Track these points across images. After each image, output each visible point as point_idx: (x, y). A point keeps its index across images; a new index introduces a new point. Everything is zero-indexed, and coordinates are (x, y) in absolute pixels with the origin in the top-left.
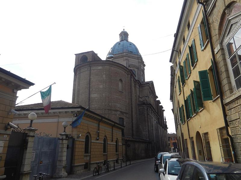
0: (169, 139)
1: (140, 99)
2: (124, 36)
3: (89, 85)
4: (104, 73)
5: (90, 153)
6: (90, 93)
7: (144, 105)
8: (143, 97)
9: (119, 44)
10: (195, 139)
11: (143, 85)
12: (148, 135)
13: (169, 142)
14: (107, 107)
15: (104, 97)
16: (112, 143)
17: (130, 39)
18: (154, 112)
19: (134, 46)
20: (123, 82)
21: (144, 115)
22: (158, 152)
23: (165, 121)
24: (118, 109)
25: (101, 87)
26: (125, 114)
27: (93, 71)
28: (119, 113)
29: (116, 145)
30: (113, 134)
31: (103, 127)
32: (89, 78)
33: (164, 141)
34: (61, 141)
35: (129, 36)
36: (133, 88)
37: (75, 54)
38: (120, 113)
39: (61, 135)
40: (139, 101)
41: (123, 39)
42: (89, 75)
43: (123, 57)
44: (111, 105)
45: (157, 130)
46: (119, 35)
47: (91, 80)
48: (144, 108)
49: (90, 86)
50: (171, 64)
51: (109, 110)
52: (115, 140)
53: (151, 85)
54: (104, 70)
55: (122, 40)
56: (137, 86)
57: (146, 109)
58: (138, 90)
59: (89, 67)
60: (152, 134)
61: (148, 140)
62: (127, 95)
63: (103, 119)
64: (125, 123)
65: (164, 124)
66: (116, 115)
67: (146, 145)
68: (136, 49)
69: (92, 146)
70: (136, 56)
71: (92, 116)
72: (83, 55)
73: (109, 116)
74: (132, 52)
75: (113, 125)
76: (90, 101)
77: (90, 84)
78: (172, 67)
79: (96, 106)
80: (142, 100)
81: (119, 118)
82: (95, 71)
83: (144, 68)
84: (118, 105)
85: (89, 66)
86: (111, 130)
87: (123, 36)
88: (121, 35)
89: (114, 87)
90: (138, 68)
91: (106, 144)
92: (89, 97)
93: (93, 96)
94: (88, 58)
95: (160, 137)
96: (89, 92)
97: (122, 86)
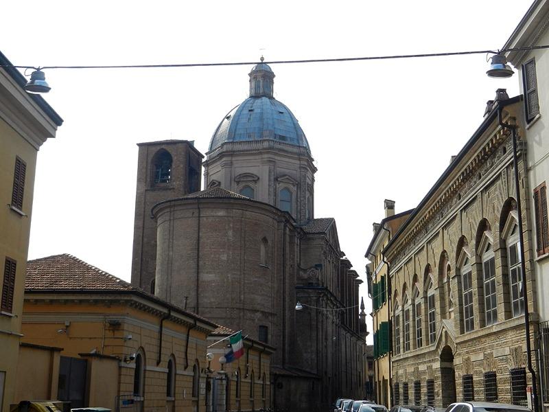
1: (301, 273)
2: (263, 82)
3: (197, 252)
5: (143, 396)
6: (200, 271)
7: (310, 291)
8: (310, 268)
9: (250, 111)
11: (311, 236)
12: (316, 362)
14: (236, 303)
15: (230, 281)
16: (157, 369)
17: (281, 92)
18: (332, 302)
19: (288, 120)
21: (310, 313)
22: (336, 399)
23: (360, 311)
24: (258, 307)
25: (224, 257)
26: (270, 318)
28: (259, 315)
29: (169, 375)
30: (161, 334)
32: (196, 236)
35: (275, 79)
36: (287, 244)
37: (138, 145)
38: (261, 315)
39: (219, 373)
40: (300, 278)
42: (197, 229)
43: (261, 153)
44: (244, 298)
45: (337, 344)
46: (250, 75)
47: (201, 241)
48: (310, 297)
49: (198, 254)
50: (368, 262)
51: (240, 309)
52: (165, 358)
53: (330, 226)
54: (230, 219)
55: (255, 96)
56: (297, 241)
57: (315, 298)
58: (296, 249)
59: (197, 210)
60: (324, 358)
61: (315, 372)
62: (275, 272)
63: (254, 345)
65: (357, 323)
67: (311, 383)
68: (299, 135)
69: (146, 387)
70: (295, 150)
72: (158, 148)
74: (283, 138)
76: (200, 289)
77: (198, 248)
79: (212, 300)
80: (306, 276)
81: (260, 326)
83: (313, 180)
84: (259, 299)
85: (196, 206)
86: (257, 358)
89: (251, 259)
90: (298, 185)
91: (142, 372)
93: (207, 277)
94: (175, 158)
95: (344, 362)
97: (267, 252)
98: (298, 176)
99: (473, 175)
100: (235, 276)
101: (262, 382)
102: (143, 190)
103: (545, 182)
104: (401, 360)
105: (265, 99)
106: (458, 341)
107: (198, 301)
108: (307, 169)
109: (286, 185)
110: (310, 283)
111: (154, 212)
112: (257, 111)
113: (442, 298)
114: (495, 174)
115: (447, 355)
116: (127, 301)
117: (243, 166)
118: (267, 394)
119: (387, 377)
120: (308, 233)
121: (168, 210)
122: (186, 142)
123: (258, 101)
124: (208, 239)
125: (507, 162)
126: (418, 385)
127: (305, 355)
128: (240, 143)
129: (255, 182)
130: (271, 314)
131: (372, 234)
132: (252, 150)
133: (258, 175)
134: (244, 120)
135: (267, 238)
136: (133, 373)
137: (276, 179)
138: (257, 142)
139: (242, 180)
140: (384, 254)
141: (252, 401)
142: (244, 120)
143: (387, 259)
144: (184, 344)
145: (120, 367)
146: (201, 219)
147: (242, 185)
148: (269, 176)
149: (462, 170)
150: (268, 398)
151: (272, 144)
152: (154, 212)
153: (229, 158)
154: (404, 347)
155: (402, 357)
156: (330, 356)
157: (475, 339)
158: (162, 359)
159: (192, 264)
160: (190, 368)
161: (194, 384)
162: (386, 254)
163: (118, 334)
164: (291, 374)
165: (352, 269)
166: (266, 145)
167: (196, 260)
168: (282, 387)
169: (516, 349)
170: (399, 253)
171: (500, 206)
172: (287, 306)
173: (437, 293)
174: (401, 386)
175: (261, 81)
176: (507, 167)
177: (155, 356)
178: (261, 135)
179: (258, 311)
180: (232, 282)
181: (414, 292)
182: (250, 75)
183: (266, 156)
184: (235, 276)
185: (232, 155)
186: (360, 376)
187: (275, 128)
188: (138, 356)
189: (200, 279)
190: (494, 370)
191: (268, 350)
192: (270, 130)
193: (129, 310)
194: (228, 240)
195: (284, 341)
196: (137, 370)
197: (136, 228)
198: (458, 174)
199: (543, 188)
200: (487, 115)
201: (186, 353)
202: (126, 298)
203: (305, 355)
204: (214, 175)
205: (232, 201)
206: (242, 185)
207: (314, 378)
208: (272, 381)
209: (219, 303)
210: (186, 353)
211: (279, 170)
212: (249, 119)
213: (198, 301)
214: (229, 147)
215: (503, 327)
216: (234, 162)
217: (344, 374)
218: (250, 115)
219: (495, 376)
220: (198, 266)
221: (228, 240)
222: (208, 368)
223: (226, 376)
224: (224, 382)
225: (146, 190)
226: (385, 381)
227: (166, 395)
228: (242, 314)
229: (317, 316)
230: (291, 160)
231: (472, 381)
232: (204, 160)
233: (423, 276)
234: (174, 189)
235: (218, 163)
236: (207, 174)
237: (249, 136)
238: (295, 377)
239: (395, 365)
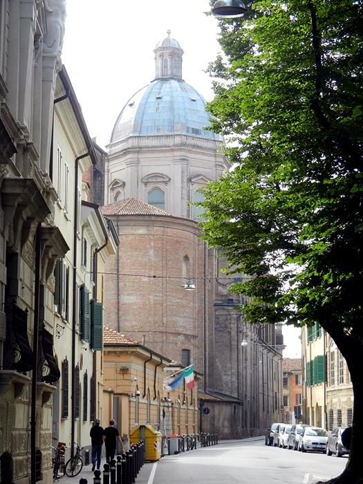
0: (285, 381)
1: (220, 288)
4: (152, 244)
6: (120, 292)
9: (158, 98)
10: (315, 410)
12: (236, 384)
13: (285, 392)
14: (159, 326)
20: (191, 259)
21: (230, 333)
24: (181, 330)
26: (192, 340)
27: (124, 237)
28: (181, 338)
43: (172, 150)
47: (121, 261)
48: (230, 315)
51: (162, 332)
57: (235, 316)
61: (236, 396)
66: (176, 344)
73: (163, 346)
75: (154, 360)
76: (121, 313)
79: (134, 323)
80: (225, 291)
81: (183, 350)
82: (130, 238)
87: (166, 60)
92: (118, 302)
93: (126, 299)
97: (188, 270)
98: (214, 175)
100: (157, 298)
101: (146, 402)
104: (335, 390)
105: (174, 83)
107: (119, 325)
108: (222, 166)
110: (229, 300)
112: (166, 98)
116: (132, 352)
117: (153, 165)
119: (322, 404)
123: (166, 85)
129: (166, 183)
130: (194, 337)
132: (161, 147)
133: (169, 175)
134: (151, 110)
137: (190, 180)
138: (167, 136)
139: (150, 180)
141: (187, 427)
142: (151, 110)
145: (130, 401)
147: (150, 187)
148: (182, 177)
150: (196, 423)
151: (184, 139)
153: (136, 155)
155: (336, 389)
156: (249, 376)
163: (126, 377)
164: (215, 399)
166: (178, 140)
175: (169, 60)
178: (172, 129)
179: (181, 334)
180: (155, 304)
182: (155, 51)
183: (177, 154)
184: (157, 298)
185: (138, 152)
186: (276, 398)
187: (187, 120)
192: (182, 123)
193: (133, 358)
202: (133, 350)
203: (224, 377)
204: (117, 173)
205: (153, 218)
206: (150, 187)
207: (235, 402)
209: (141, 327)
211: (194, 170)
212: (157, 109)
213: (119, 325)
214: (135, 143)
216: (142, 160)
217: (261, 396)
218: (159, 104)
221: (149, 260)
226: (318, 408)
228: (164, 337)
229: (238, 335)
230: (205, 158)
235: (122, 159)
237: (158, 130)
238: (219, 401)
239: (330, 394)
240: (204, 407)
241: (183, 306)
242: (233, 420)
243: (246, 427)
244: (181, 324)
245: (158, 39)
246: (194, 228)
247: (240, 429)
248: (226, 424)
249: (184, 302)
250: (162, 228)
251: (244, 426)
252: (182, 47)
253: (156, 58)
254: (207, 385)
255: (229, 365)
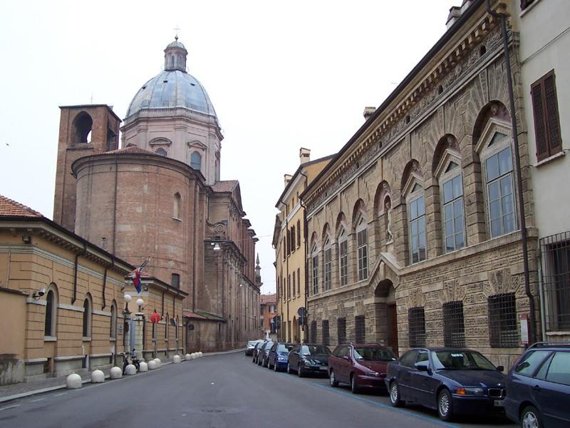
4: (147, 180)
5: (57, 336)
11: (219, 195)
13: (262, 317)
20: (182, 198)
23: (256, 265)
25: (139, 210)
27: (122, 174)
28: (172, 264)
29: (85, 314)
31: (86, 269)
32: (113, 189)
33: (251, 317)
34: (137, 322)
37: (60, 107)
38: (173, 264)
41: (175, 65)
42: (114, 183)
47: (118, 194)
49: (115, 206)
50: (278, 211)
52: (81, 297)
54: (146, 174)
56: (205, 198)
58: (205, 206)
63: (116, 264)
64: (181, 284)
70: (205, 119)
71: (63, 240)
72: (80, 111)
76: (117, 240)
77: (115, 201)
78: (277, 217)
79: (129, 249)
81: (173, 274)
82: (127, 174)
86: (71, 264)
87: (173, 57)
88: (168, 50)
96: (115, 220)
99: (431, 90)
102: (66, 146)
103: (553, 70)
106: (402, 273)
109: (197, 150)
111: (74, 167)
113: (377, 232)
114: (467, 80)
115: (385, 289)
118: (180, 335)
120: (216, 193)
121: (87, 165)
122: (105, 106)
123: (172, 74)
124: (124, 193)
125: (489, 61)
126: (342, 323)
127: (212, 300)
128: (156, 110)
129: (168, 145)
130: (183, 263)
131: (363, 121)
135: (180, 193)
136: (44, 310)
138: (171, 109)
140: (301, 197)
143: (305, 203)
144: (102, 283)
146: (118, 173)
149: (417, 86)
152: (74, 167)
154: (323, 287)
155: (321, 296)
157: (432, 267)
158: (77, 297)
159: (110, 216)
160: (108, 308)
161: (111, 324)
162: (304, 198)
165: (250, 228)
167: (113, 212)
168: (193, 329)
169: (499, 274)
170: (319, 195)
171: (472, 116)
172: (197, 257)
173: (371, 229)
174: (320, 328)
176: (487, 68)
177: (70, 294)
180: (147, 233)
181: (325, 239)
188: (50, 293)
189: (117, 230)
190: (459, 299)
191: (182, 295)
194: (143, 194)
195: (194, 287)
196: (49, 307)
197: (57, 184)
198: (410, 92)
199: (549, 79)
200: (452, 22)
201: (103, 292)
203: (212, 300)
205: (148, 158)
208: (185, 323)
209: (134, 253)
210: (103, 292)
215: (434, 264)
217: (243, 318)
219: (462, 306)
220: (115, 217)
221: (143, 194)
222: (127, 309)
223: (144, 318)
224: (141, 323)
225: (67, 150)
227: (82, 335)
231: (424, 314)
232: (122, 124)
233: (352, 212)
234: (93, 148)
235: (134, 128)
236: (124, 139)
240: (189, 324)
241: (173, 236)
242: (218, 335)
243: (231, 340)
244: (172, 251)
245: (170, 40)
246: (185, 171)
247: (224, 343)
248: (212, 339)
249: (175, 233)
250: (156, 167)
251: (229, 339)
252: (186, 48)
253: (165, 56)
254: (196, 306)
255: (215, 291)
